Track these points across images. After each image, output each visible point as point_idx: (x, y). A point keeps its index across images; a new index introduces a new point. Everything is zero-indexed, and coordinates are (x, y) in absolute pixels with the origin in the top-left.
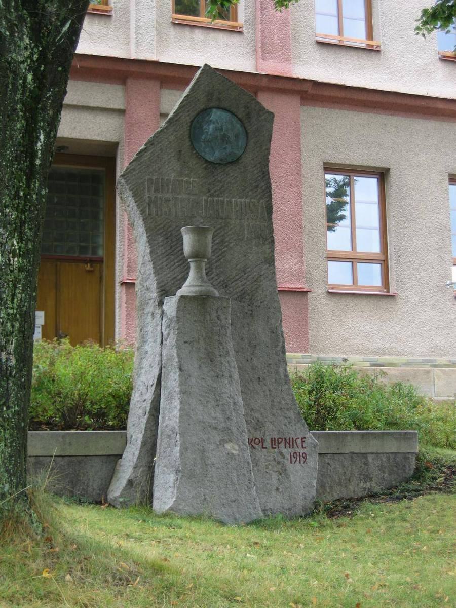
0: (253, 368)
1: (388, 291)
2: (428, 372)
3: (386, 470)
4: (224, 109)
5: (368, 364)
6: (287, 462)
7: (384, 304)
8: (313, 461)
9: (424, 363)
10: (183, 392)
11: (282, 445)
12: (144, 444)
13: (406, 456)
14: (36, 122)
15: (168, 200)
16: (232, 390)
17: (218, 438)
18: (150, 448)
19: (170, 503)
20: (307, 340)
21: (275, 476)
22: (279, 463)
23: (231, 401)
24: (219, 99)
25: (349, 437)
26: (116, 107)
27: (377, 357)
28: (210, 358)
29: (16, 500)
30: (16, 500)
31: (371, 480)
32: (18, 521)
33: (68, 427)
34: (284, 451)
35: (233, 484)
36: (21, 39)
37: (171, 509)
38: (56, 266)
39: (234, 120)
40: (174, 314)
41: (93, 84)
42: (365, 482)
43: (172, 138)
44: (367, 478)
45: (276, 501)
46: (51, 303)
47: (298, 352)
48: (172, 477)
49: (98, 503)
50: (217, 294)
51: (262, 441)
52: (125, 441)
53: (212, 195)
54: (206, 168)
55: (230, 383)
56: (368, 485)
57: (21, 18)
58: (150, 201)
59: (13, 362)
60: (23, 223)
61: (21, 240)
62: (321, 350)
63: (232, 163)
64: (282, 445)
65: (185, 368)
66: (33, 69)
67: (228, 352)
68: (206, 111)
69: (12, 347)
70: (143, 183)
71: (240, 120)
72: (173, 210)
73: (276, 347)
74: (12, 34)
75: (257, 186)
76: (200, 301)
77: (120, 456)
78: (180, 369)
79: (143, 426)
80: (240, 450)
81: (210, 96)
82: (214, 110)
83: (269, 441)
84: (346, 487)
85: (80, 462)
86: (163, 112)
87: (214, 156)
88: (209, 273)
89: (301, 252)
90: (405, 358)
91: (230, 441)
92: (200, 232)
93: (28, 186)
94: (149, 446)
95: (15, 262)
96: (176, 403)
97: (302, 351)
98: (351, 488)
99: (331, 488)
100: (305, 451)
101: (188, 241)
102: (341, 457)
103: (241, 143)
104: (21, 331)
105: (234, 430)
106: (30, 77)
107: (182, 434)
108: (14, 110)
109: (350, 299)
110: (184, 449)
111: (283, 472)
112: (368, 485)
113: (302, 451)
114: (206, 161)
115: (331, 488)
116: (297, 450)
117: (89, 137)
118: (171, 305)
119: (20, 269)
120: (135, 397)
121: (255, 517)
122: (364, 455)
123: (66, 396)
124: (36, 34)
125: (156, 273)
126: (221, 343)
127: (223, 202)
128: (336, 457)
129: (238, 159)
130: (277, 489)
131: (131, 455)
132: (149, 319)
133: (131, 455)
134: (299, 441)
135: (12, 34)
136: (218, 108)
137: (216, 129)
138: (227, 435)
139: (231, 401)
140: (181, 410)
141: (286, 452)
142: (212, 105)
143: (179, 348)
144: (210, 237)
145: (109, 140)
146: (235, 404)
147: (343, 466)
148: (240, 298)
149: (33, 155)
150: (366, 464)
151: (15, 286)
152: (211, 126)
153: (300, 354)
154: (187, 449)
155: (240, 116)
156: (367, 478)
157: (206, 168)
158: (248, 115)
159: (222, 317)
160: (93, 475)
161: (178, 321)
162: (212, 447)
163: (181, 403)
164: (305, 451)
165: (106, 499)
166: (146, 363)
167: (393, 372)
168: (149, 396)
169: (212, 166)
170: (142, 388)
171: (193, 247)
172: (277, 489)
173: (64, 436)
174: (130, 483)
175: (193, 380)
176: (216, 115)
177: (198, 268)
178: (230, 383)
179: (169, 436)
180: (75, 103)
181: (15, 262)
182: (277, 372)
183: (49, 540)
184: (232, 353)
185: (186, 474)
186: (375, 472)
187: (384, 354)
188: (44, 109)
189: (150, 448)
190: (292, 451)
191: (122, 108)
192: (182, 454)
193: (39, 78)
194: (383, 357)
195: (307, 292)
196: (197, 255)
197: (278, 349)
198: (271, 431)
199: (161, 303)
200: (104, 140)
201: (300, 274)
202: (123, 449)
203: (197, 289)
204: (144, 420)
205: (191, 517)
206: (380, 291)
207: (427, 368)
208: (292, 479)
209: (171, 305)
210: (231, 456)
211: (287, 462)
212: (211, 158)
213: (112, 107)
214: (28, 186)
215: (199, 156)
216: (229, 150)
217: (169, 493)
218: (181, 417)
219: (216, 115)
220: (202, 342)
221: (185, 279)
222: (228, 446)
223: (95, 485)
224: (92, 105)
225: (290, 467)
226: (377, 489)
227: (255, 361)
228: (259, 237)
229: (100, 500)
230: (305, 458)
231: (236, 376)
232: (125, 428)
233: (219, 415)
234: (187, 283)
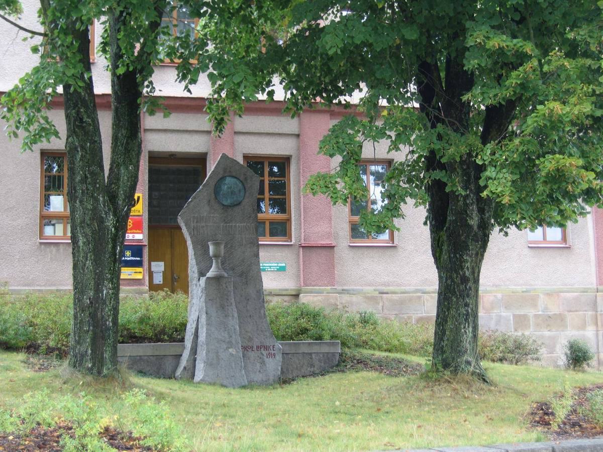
0: (247, 311)
1: (393, 243)
2: (420, 297)
3: (323, 362)
4: (233, 177)
5: (378, 292)
6: (265, 358)
7: (389, 252)
8: (279, 357)
9: (417, 291)
10: (208, 324)
11: (262, 349)
12: (192, 349)
13: (333, 354)
14: (116, 243)
15: (203, 227)
16: (234, 323)
17: (225, 347)
18: (194, 351)
19: (201, 377)
20: (334, 278)
21: (258, 365)
22: (260, 358)
23: (232, 328)
24: (230, 171)
25: (302, 345)
26: (206, 129)
27: (384, 288)
28: (222, 307)
29: (113, 370)
30: (113, 370)
31: (314, 367)
32: (113, 377)
33: (159, 340)
34: (263, 352)
35: (232, 368)
36: (110, 217)
37: (201, 380)
38: (171, 232)
39: (238, 182)
40: (204, 286)
41: (190, 115)
42: (311, 367)
43: (205, 194)
44: (312, 365)
45: (258, 377)
46: (168, 256)
47: (327, 286)
48: (202, 365)
49: (170, 378)
50: (226, 275)
51: (252, 347)
52: (184, 347)
53: (226, 223)
54: (223, 209)
55: (233, 319)
56: (312, 369)
57: (109, 209)
58: (194, 228)
59: (111, 324)
60: (113, 279)
61: (112, 284)
62: (345, 285)
63: (237, 205)
64: (262, 349)
65: (209, 312)
66: (115, 227)
67: (232, 304)
68: (223, 179)
69: (110, 320)
70: (190, 219)
71: (241, 182)
72: (206, 232)
73: (260, 299)
74: (106, 216)
75: (250, 217)
76: (217, 279)
77: (181, 355)
78: (207, 313)
79: (191, 341)
80: (237, 352)
81: (225, 170)
82: (227, 178)
83: (256, 347)
84: (300, 371)
85: (162, 359)
86: (236, 131)
87: (227, 202)
88: (223, 264)
89: (330, 220)
90: (404, 288)
91: (232, 348)
92: (217, 244)
93: (114, 265)
94: (194, 351)
95: (111, 292)
96: (205, 329)
97: (331, 285)
98: (303, 371)
99: (292, 371)
100: (275, 352)
101: (211, 249)
102: (297, 355)
103: (242, 194)
104: (113, 314)
105: (234, 342)
106: (113, 229)
107: (207, 345)
108: (108, 241)
109: (365, 250)
110: (208, 352)
111: (263, 363)
112: (312, 369)
113: (273, 352)
114: (223, 205)
115: (292, 371)
116: (270, 352)
117: (188, 150)
118: (203, 280)
119: (112, 294)
120: (188, 326)
121: (243, 384)
122: (311, 354)
123: (550, 182)
124: (115, 215)
125: (197, 264)
126: (228, 300)
127: (232, 226)
128: (295, 355)
129: (240, 203)
130: (260, 371)
131: (186, 354)
132: (195, 287)
133: (186, 354)
134: (271, 347)
135: (106, 216)
136: (230, 176)
137: (228, 188)
138: (230, 345)
139: (232, 328)
140: (206, 333)
141: (265, 353)
142: (226, 175)
143: (206, 302)
144: (222, 247)
145: (200, 151)
146: (235, 329)
147: (299, 360)
148: (241, 275)
149: (115, 255)
150: (311, 358)
151: (111, 300)
152: (226, 186)
153: (329, 288)
154: (209, 352)
155: (241, 179)
156: (312, 365)
157: (223, 209)
158: (246, 179)
159: (228, 287)
160: (168, 365)
161: (206, 290)
162: (222, 350)
163: (207, 329)
164: (275, 352)
165: (174, 377)
166: (193, 309)
167: (395, 298)
168: (194, 326)
169: (226, 207)
170: (191, 322)
171: (214, 252)
172: (260, 371)
173: (153, 346)
174: (185, 368)
175: (213, 319)
176: (229, 180)
177: (217, 262)
178: (233, 319)
179: (202, 346)
180: (178, 129)
181: (111, 292)
182: (260, 312)
183: (124, 383)
184: (234, 304)
185: (209, 364)
186: (317, 363)
187: (389, 286)
188: (119, 238)
189: (194, 351)
190: (267, 352)
191: (209, 130)
192: (207, 354)
193: (116, 228)
194: (388, 288)
195: (334, 247)
196: (216, 256)
197: (260, 301)
198: (256, 342)
199: (199, 280)
200: (198, 151)
201: (329, 235)
202: (183, 352)
203: (215, 273)
204: (192, 338)
205: (210, 384)
206: (387, 243)
207: (419, 294)
208: (267, 365)
209: (203, 280)
210: (232, 355)
211: (265, 358)
212: (225, 203)
213: (200, 130)
214: (114, 265)
215: (219, 203)
216: (235, 199)
217: (201, 373)
218: (206, 336)
219: (229, 180)
220: (218, 299)
221: (211, 266)
222: (230, 350)
223: (169, 369)
224: (189, 129)
225: (266, 360)
226: (317, 372)
227: (248, 308)
228: (251, 243)
229: (171, 376)
230: (275, 356)
231: (236, 315)
232: (184, 342)
233: (226, 335)
234: (211, 270)
